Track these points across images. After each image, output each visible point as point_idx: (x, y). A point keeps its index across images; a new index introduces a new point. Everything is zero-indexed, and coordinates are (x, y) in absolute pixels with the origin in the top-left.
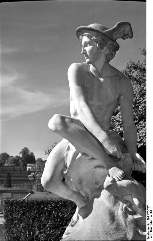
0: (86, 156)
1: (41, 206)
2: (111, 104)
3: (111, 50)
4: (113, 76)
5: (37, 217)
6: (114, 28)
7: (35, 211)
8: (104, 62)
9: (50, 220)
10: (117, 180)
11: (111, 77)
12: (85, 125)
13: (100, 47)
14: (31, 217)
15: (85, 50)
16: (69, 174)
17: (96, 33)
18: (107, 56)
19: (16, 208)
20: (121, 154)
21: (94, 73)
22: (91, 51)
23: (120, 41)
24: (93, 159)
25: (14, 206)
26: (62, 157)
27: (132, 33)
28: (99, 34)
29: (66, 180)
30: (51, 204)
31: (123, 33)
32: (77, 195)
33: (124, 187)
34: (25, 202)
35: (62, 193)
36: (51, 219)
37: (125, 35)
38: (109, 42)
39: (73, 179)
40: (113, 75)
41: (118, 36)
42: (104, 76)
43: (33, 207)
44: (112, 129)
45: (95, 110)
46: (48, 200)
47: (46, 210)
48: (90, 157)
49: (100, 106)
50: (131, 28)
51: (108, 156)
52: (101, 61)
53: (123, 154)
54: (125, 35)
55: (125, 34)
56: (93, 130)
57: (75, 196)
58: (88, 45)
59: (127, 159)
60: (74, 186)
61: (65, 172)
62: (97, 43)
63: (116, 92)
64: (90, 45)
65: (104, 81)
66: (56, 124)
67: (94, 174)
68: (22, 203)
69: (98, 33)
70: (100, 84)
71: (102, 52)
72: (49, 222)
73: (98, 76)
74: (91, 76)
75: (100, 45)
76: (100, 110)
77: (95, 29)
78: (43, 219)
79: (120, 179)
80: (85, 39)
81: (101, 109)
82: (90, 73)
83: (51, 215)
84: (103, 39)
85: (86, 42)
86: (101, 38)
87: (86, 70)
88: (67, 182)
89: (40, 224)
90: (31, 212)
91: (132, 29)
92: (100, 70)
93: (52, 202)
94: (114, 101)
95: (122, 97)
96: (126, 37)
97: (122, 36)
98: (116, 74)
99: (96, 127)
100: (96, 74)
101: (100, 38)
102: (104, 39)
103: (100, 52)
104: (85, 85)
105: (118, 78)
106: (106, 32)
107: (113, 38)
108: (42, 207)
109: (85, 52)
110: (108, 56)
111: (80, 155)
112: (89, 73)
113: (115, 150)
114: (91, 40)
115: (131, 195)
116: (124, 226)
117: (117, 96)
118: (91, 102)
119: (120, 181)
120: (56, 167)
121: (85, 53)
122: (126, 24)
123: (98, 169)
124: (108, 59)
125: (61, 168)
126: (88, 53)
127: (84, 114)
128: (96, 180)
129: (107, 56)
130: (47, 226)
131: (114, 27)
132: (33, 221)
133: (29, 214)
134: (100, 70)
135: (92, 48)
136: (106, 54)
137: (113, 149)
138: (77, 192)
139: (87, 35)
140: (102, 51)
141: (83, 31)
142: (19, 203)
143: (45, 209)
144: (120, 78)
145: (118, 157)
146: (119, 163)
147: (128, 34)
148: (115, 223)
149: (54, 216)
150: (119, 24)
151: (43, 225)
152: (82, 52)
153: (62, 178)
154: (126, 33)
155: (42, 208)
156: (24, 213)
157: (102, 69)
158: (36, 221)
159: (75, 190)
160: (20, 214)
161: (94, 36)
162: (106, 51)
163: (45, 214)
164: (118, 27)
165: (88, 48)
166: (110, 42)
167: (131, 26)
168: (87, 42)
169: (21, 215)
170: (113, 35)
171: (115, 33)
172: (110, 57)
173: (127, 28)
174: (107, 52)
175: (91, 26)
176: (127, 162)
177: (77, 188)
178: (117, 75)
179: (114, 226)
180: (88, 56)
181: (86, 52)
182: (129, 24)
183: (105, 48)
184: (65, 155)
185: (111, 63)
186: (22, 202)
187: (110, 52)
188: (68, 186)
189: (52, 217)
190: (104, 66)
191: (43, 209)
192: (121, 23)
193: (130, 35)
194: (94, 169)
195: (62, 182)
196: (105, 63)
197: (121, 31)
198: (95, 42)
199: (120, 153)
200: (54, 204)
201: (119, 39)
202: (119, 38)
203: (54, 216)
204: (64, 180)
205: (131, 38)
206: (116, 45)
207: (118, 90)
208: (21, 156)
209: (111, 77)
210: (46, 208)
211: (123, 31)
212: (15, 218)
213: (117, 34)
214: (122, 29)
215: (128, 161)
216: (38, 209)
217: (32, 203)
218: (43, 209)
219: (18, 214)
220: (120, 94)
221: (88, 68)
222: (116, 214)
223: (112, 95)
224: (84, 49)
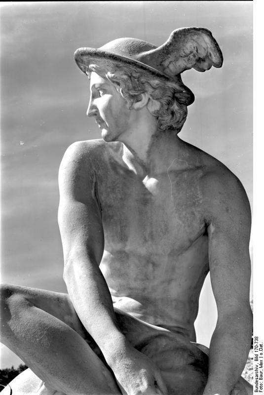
2: (183, 249)
4: (185, 170)
6: (166, 45)
12: (77, 312)
13: (127, 95)
15: (94, 107)
17: (111, 62)
21: (131, 167)
22: (108, 109)
23: (191, 78)
28: (121, 64)
40: (186, 165)
42: (158, 171)
49: (151, 254)
50: (214, 41)
54: (200, 60)
55: (200, 58)
56: (91, 325)
62: (118, 86)
63: (193, 213)
64: (105, 92)
65: (158, 185)
69: (116, 63)
70: (145, 197)
73: (142, 173)
74: (122, 172)
75: (127, 90)
76: (150, 267)
77: (117, 54)
80: (95, 79)
81: (154, 264)
82: (120, 166)
86: (125, 74)
87: (111, 158)
91: (217, 45)
92: (143, 155)
96: (206, 64)
97: (194, 63)
98: (198, 164)
99: (99, 317)
100: (136, 168)
102: (134, 75)
104: (103, 197)
105: (200, 173)
106: (143, 59)
107: (167, 70)
109: (94, 110)
110: (160, 118)
112: (116, 166)
114: (104, 78)
117: (198, 227)
118: (125, 246)
121: (96, 115)
126: (102, 115)
127: (74, 280)
131: (164, 44)
134: (143, 155)
135: (110, 101)
139: (94, 70)
140: (137, 105)
141: (85, 58)
144: (207, 174)
150: (175, 34)
154: (202, 54)
157: (149, 152)
161: (108, 71)
164: (176, 41)
165: (101, 102)
166: (156, 82)
168: (96, 86)
170: (166, 63)
171: (171, 58)
175: (109, 47)
178: (198, 168)
180: (103, 121)
181: (97, 111)
182: (209, 34)
183: (145, 98)
192: (180, 31)
193: (215, 59)
198: (116, 85)
205: (219, 65)
207: (199, 209)
208: (143, 371)
209: (178, 173)
211: (195, 52)
214: (189, 46)
220: (205, 220)
221: (119, 153)
223: (181, 223)
224: (92, 104)
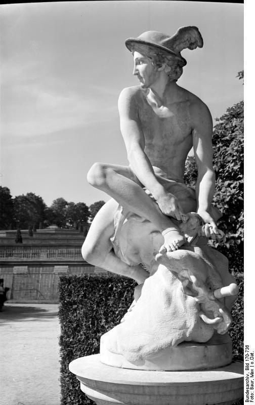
0: (138, 218)
1: (108, 285)
2: (181, 142)
3: (173, 67)
5: (103, 300)
7: (100, 292)
8: (166, 83)
9: (120, 305)
10: (168, 249)
11: (178, 104)
14: (94, 300)
16: (116, 241)
17: (148, 46)
18: (169, 75)
19: (75, 287)
20: (181, 214)
22: (145, 71)
23: (186, 53)
24: (146, 221)
25: (73, 285)
26: (111, 220)
27: (202, 40)
28: (153, 48)
29: (115, 250)
30: (122, 282)
31: (189, 42)
32: (135, 270)
33: (176, 260)
34: (87, 279)
35: (110, 266)
36: (123, 303)
37: (192, 44)
38: (168, 57)
39: (124, 249)
40: (181, 100)
41: (182, 45)
42: (168, 103)
43: (98, 286)
44: (223, 168)
45: (159, 151)
46: (118, 276)
47: (115, 290)
48: (144, 219)
49: (165, 145)
50: (199, 33)
51: (165, 217)
52: (162, 83)
53: (184, 215)
54: (192, 44)
57: (132, 272)
58: (141, 63)
59: (191, 220)
60: (125, 258)
61: (112, 239)
63: (186, 124)
64: (143, 62)
66: (94, 177)
67: (152, 241)
68: (83, 281)
71: (160, 71)
72: (120, 308)
77: (147, 41)
78: (111, 303)
79: (173, 249)
83: (122, 297)
84: (158, 55)
85: (137, 58)
88: (117, 252)
89: (107, 310)
90: (95, 293)
93: (123, 279)
94: (184, 138)
95: (195, 132)
96: (194, 46)
97: (188, 45)
98: (187, 99)
101: (154, 52)
102: (160, 54)
103: (157, 71)
104: (142, 118)
105: (189, 104)
108: (110, 286)
111: (126, 220)
113: (174, 208)
115: (187, 270)
116: (184, 311)
117: (188, 131)
119: (172, 251)
120: (102, 233)
122: (192, 29)
123: (154, 234)
124: (172, 81)
125: (108, 234)
126: (141, 75)
128: (155, 250)
129: (169, 75)
130: (117, 312)
132: (98, 306)
133: (92, 295)
135: (146, 68)
136: (168, 73)
137: (171, 208)
138: (133, 266)
140: (160, 69)
142: (78, 280)
143: (114, 289)
145: (179, 219)
146: (181, 226)
147: (196, 42)
148: (172, 306)
149: (126, 299)
151: (112, 311)
152: (133, 73)
153: (111, 248)
154: (193, 40)
155: (110, 288)
156: (85, 294)
157: (164, 94)
158: (102, 306)
159: (128, 263)
160: (80, 296)
162: (166, 69)
163: (114, 296)
164: (180, 34)
166: (170, 57)
167: (199, 30)
169: (82, 297)
171: (177, 43)
172: (174, 76)
173: (194, 35)
174: (169, 70)
176: (191, 225)
177: (130, 261)
178: (188, 101)
179: (170, 310)
182: (196, 29)
183: (164, 65)
184: (115, 217)
185: (179, 83)
186: (83, 280)
187: (172, 69)
188: (119, 258)
189: (123, 300)
190: (166, 90)
191: (111, 288)
193: (199, 44)
194: (151, 236)
195: (111, 253)
196: (168, 85)
197: (185, 39)
199: (179, 214)
200: (126, 283)
201: (184, 50)
202: (185, 48)
203: (126, 299)
204: (113, 250)
205: (201, 46)
206: (180, 59)
209: (178, 104)
210: (116, 287)
212: (74, 301)
213: (180, 44)
214: (186, 36)
215: (193, 224)
216: (105, 290)
217: (95, 280)
218: (111, 288)
219: (78, 295)
220: (191, 128)
222: (173, 295)
